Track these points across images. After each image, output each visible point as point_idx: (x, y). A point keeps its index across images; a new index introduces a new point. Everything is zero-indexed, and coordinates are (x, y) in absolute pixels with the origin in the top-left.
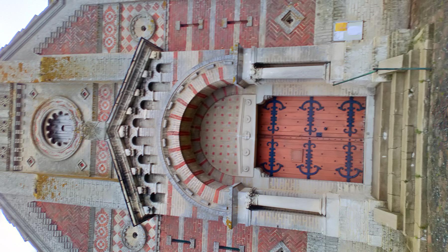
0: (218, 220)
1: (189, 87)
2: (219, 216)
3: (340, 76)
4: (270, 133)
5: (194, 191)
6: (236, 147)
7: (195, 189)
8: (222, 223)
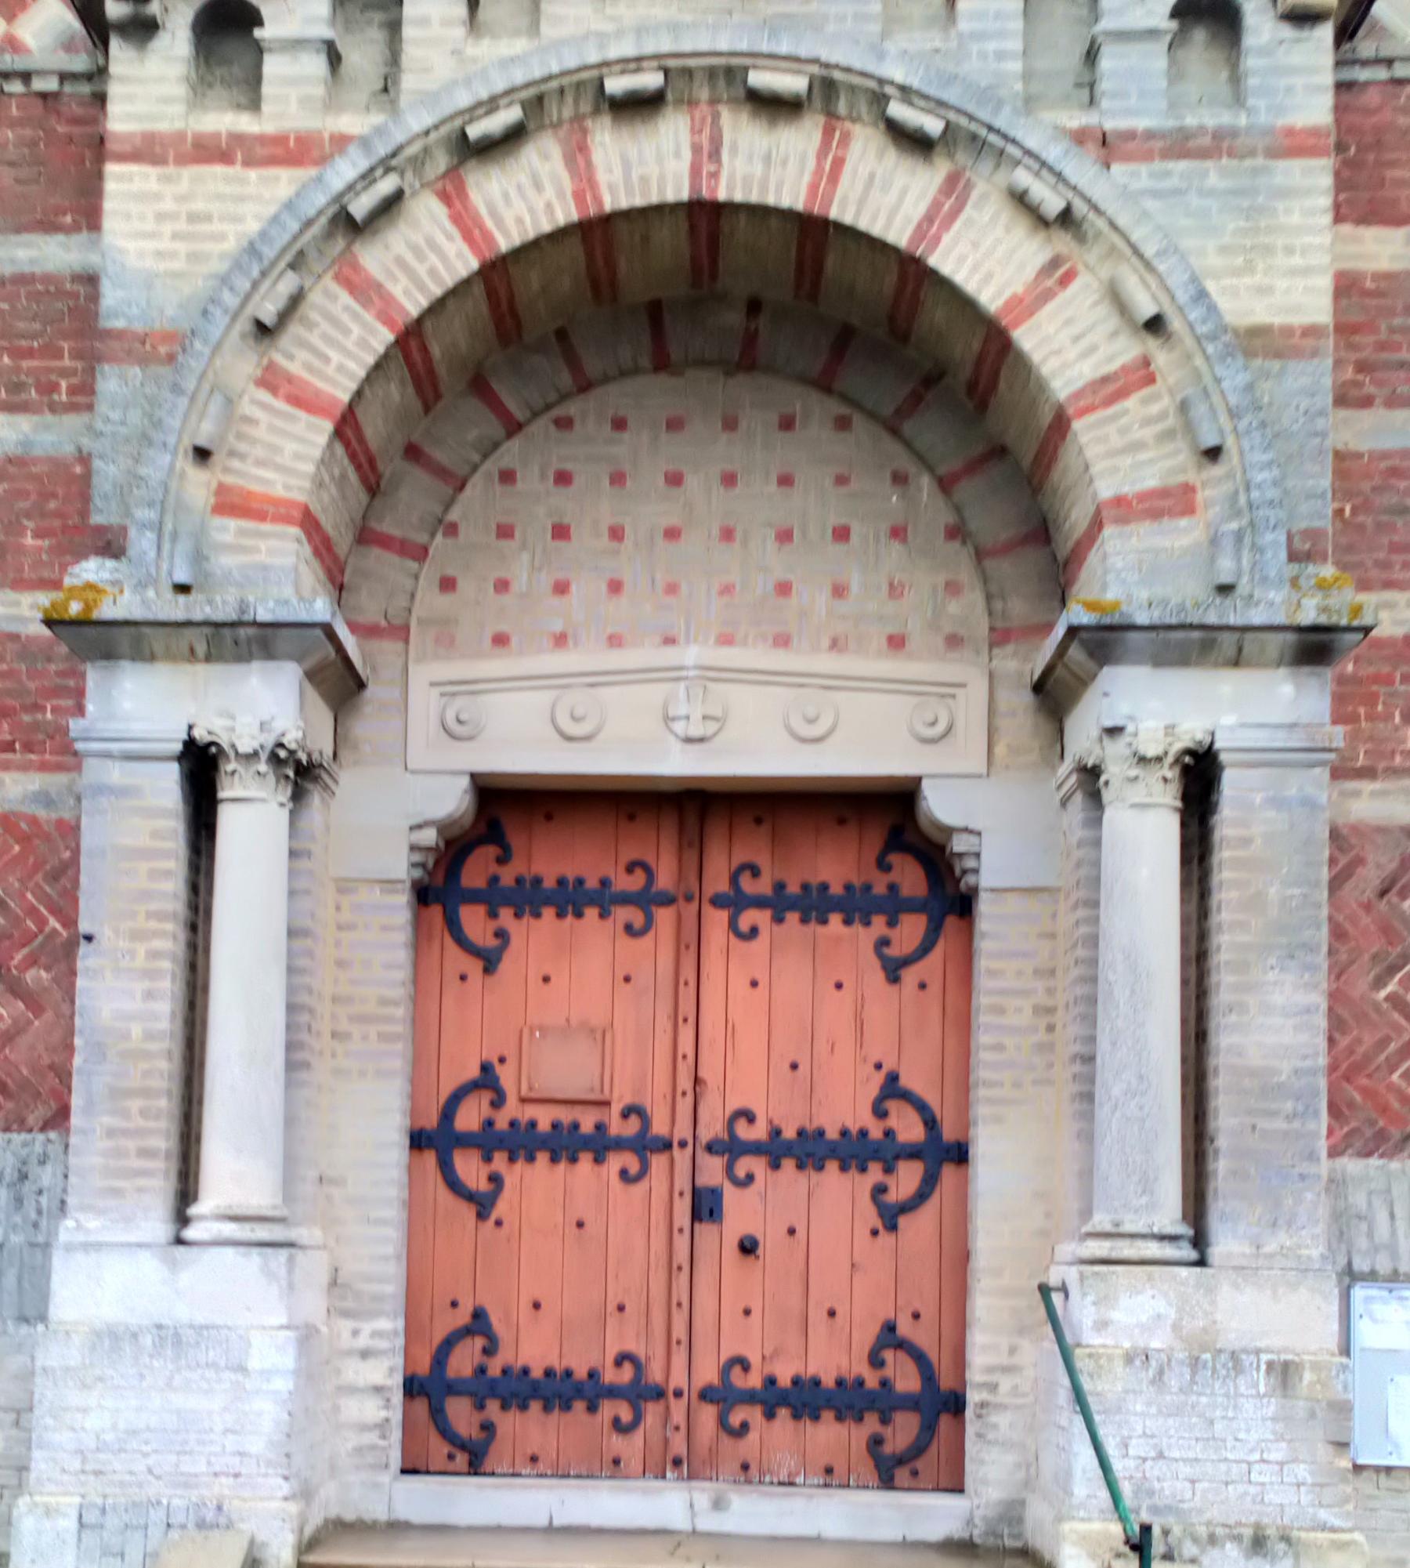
0: (96, 519)
1: (1055, 263)
2: (124, 530)
3: (1102, 1325)
4: (717, 881)
5: (285, 340)
6: (615, 641)
7: (304, 344)
8: (81, 555)
